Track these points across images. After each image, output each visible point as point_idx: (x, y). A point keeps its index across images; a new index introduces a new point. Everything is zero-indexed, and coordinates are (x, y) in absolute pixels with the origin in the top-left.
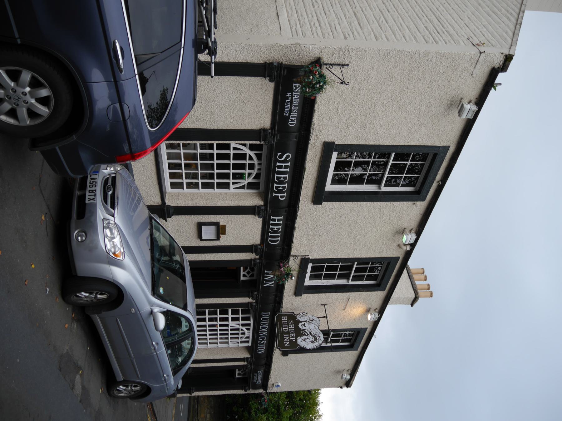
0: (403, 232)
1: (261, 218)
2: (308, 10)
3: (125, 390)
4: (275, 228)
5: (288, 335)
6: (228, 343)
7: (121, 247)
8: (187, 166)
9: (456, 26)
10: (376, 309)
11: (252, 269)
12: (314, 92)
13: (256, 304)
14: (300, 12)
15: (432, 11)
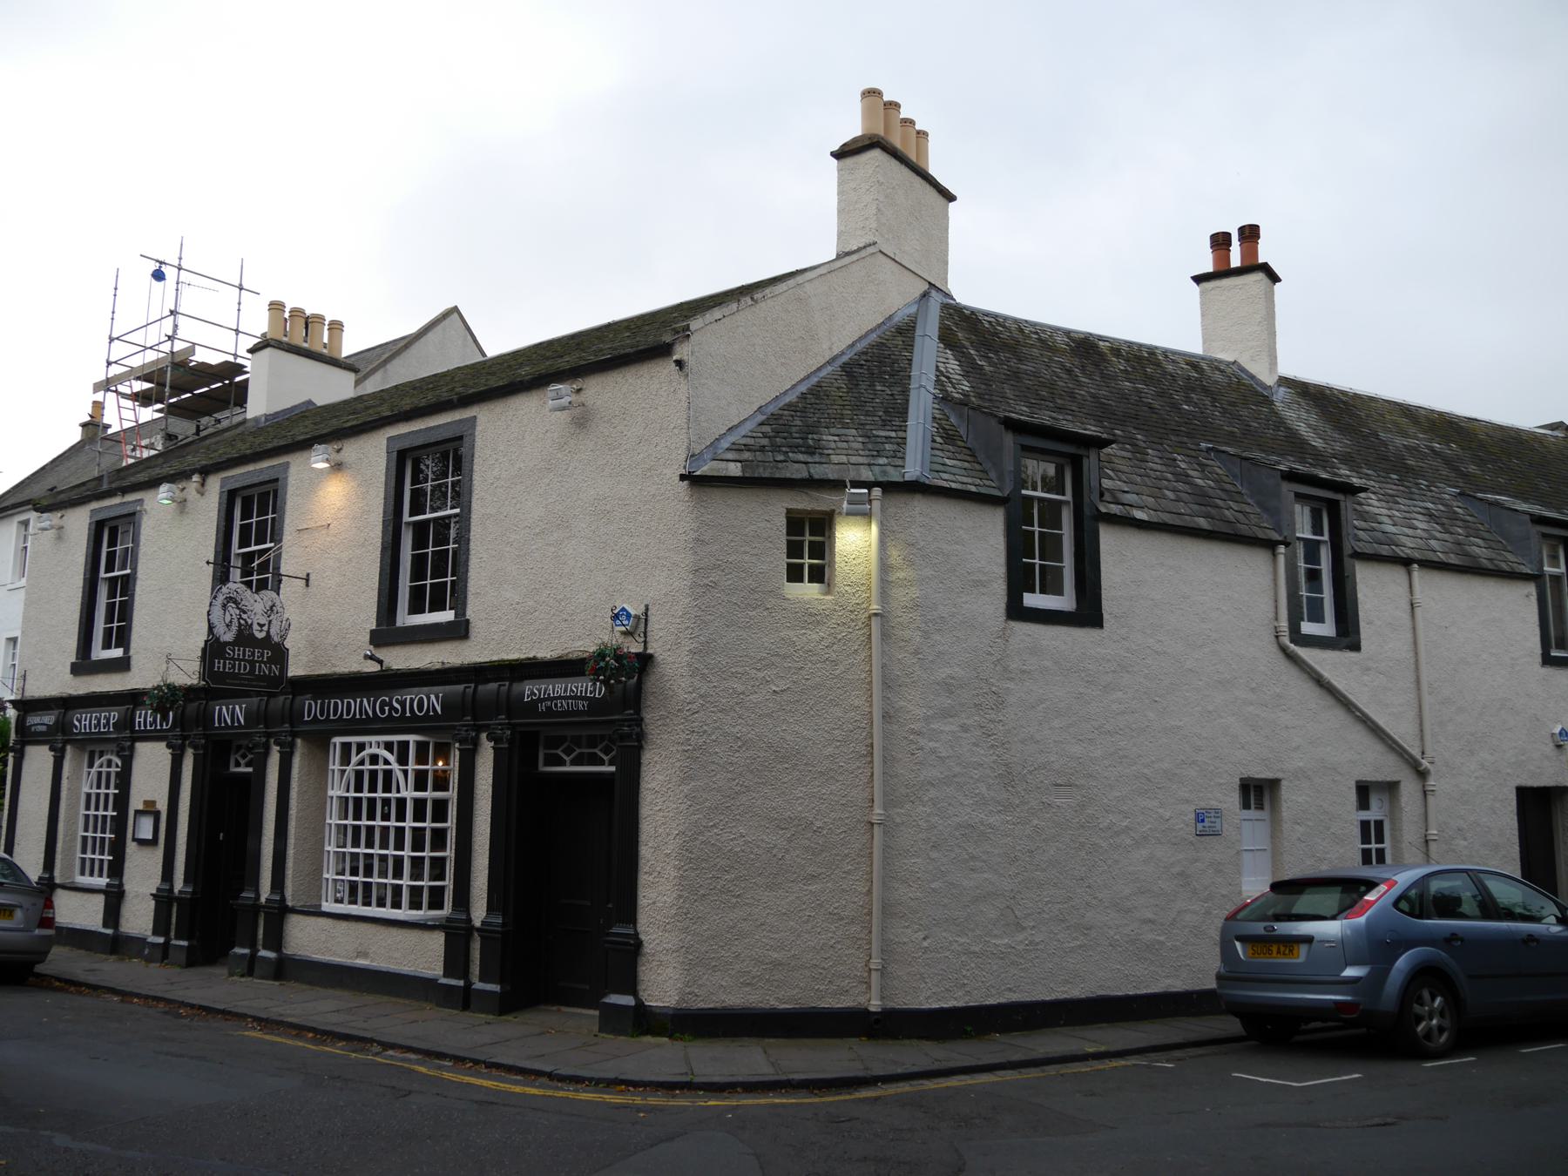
5: (257, 664)
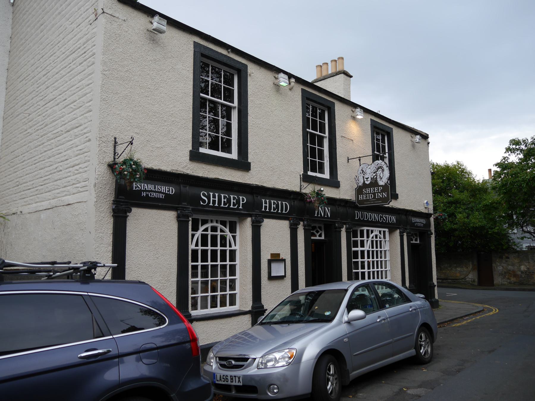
0: (278, 85)
1: (263, 220)
2: (64, 176)
3: (424, 348)
4: (274, 207)
5: (377, 194)
6: (385, 251)
7: (284, 351)
8: (214, 290)
9: (78, 36)
10: (352, 110)
11: (314, 228)
12: (140, 170)
13: (347, 224)
14: (66, 184)
15: (66, 58)
